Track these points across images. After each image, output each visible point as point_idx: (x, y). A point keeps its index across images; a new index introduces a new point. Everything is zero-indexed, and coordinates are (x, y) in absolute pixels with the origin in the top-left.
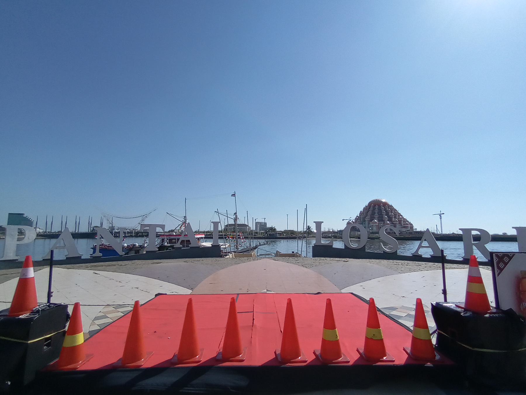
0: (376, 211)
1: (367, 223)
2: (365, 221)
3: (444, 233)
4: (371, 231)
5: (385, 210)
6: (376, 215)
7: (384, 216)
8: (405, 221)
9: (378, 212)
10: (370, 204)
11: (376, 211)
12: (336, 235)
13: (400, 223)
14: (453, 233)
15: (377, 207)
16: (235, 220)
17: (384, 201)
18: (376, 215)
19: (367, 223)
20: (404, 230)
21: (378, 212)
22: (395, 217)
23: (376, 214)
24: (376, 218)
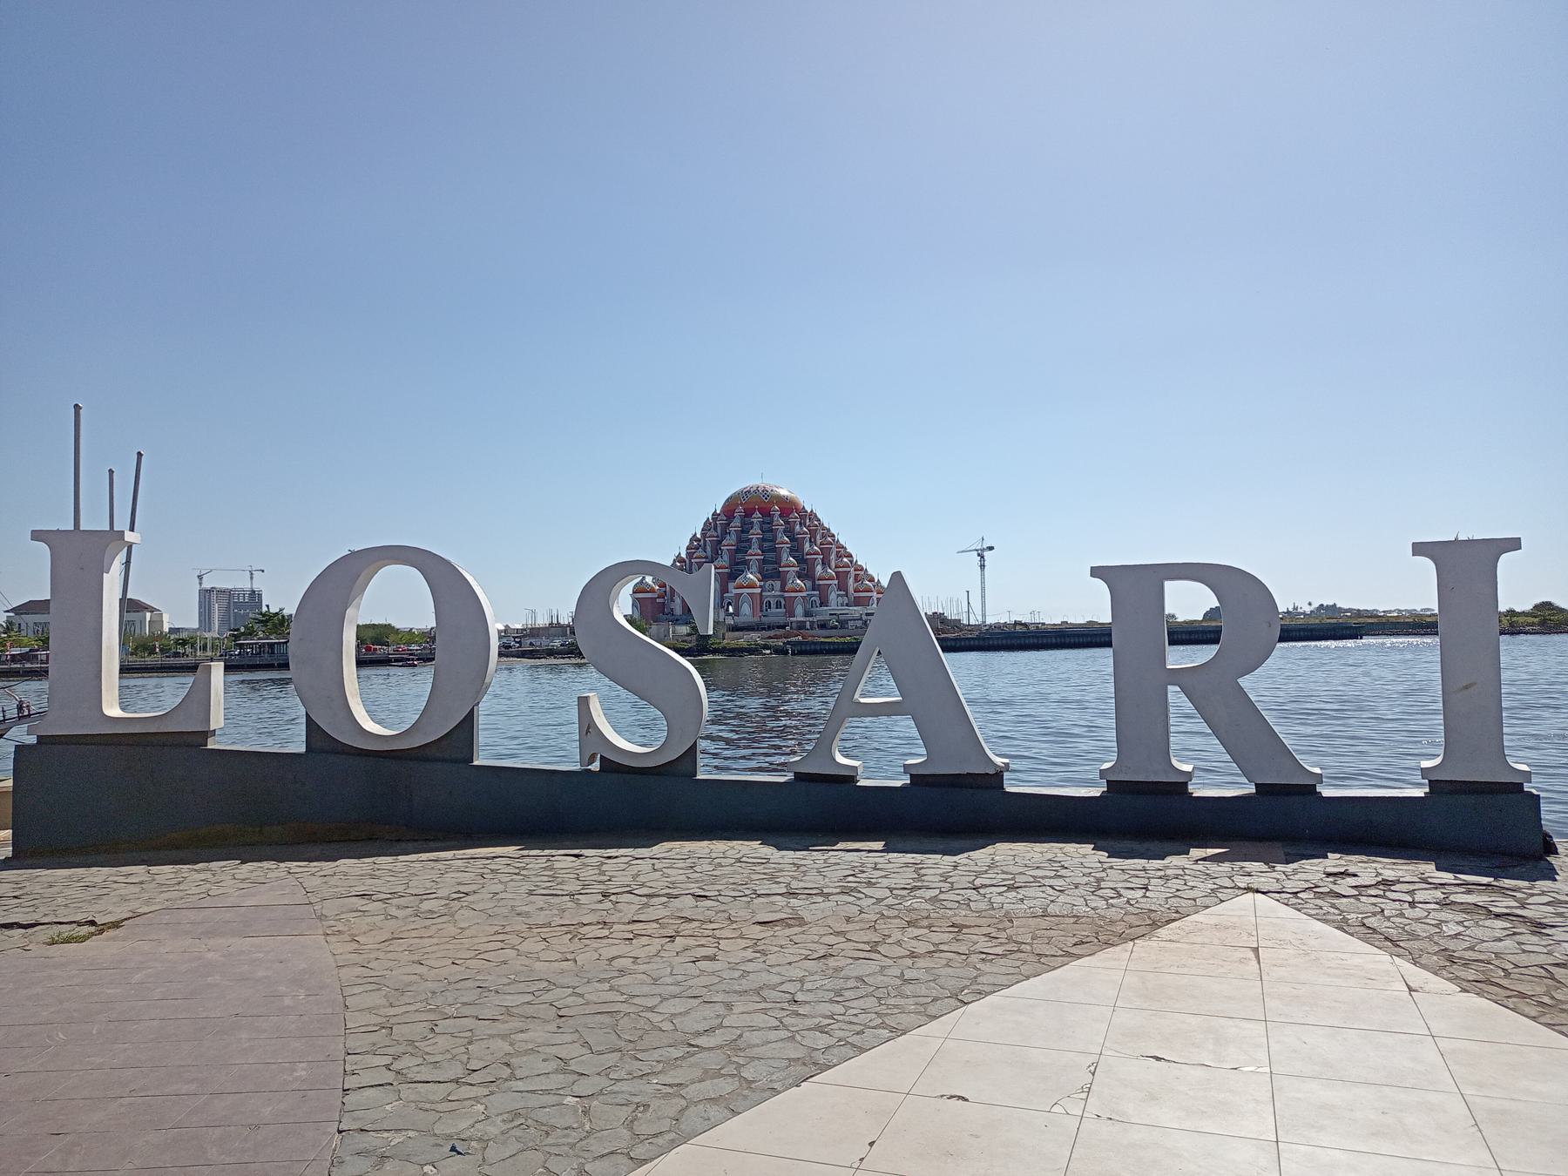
0: (755, 534)
4: (730, 621)
6: (754, 554)
9: (760, 532)
11: (755, 534)
17: (783, 492)
18: (754, 554)
21: (760, 532)
22: (826, 563)
24: (754, 569)
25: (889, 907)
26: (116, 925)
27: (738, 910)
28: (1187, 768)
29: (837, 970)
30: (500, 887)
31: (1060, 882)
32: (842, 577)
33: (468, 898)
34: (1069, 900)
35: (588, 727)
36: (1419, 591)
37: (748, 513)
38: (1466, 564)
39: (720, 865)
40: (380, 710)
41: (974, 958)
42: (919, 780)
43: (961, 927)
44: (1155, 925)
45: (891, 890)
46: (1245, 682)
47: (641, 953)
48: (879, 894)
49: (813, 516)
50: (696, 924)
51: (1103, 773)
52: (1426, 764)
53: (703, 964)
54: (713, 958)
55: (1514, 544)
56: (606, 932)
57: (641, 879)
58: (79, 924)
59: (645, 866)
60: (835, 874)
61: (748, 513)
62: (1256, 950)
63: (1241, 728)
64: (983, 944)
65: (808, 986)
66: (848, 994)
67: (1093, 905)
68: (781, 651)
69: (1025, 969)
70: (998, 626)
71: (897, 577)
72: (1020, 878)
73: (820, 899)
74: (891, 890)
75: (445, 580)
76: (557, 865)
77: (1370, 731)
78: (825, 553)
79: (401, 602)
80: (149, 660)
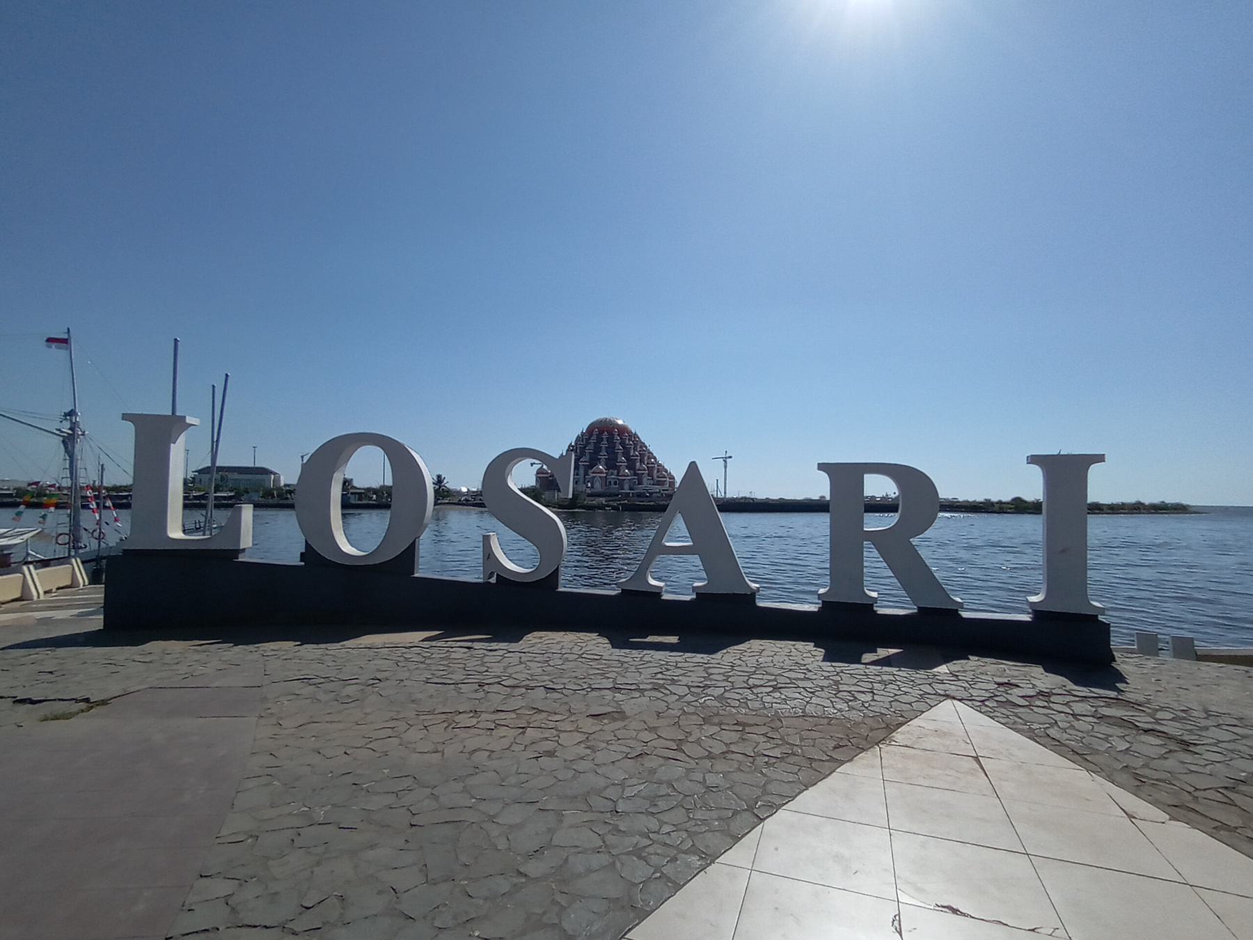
0: (604, 444)
4: (589, 491)
6: (603, 455)
8: (661, 468)
9: (606, 445)
11: (604, 444)
17: (620, 422)
18: (603, 455)
20: (657, 488)
21: (606, 445)
22: (642, 461)
24: (603, 461)
25: (689, 703)
26: (104, 703)
27: (577, 705)
28: (874, 595)
29: (653, 771)
30: (407, 674)
31: (808, 684)
32: (650, 469)
33: (381, 685)
34: (818, 701)
35: (489, 555)
36: (1032, 487)
37: (601, 432)
38: (1066, 472)
39: (567, 660)
40: (351, 541)
41: (761, 761)
42: (702, 596)
43: (745, 725)
44: (891, 728)
45: (689, 687)
46: (915, 541)
47: (497, 746)
48: (682, 691)
49: (636, 435)
50: (544, 715)
51: (820, 596)
52: (1033, 599)
53: (544, 761)
54: (551, 754)
55: (1100, 458)
56: (474, 721)
57: (510, 670)
58: (77, 701)
59: (514, 658)
60: (647, 673)
61: (601, 432)
62: (976, 759)
63: (911, 571)
64: (764, 746)
65: (629, 792)
66: (662, 805)
67: (838, 706)
68: (614, 508)
69: (802, 776)
70: (733, 499)
71: (693, 467)
72: (781, 680)
73: (638, 694)
74: (689, 687)
75: (398, 455)
76: (453, 656)
77: (995, 577)
78: (642, 456)
79: (369, 470)
80: (271, 501)
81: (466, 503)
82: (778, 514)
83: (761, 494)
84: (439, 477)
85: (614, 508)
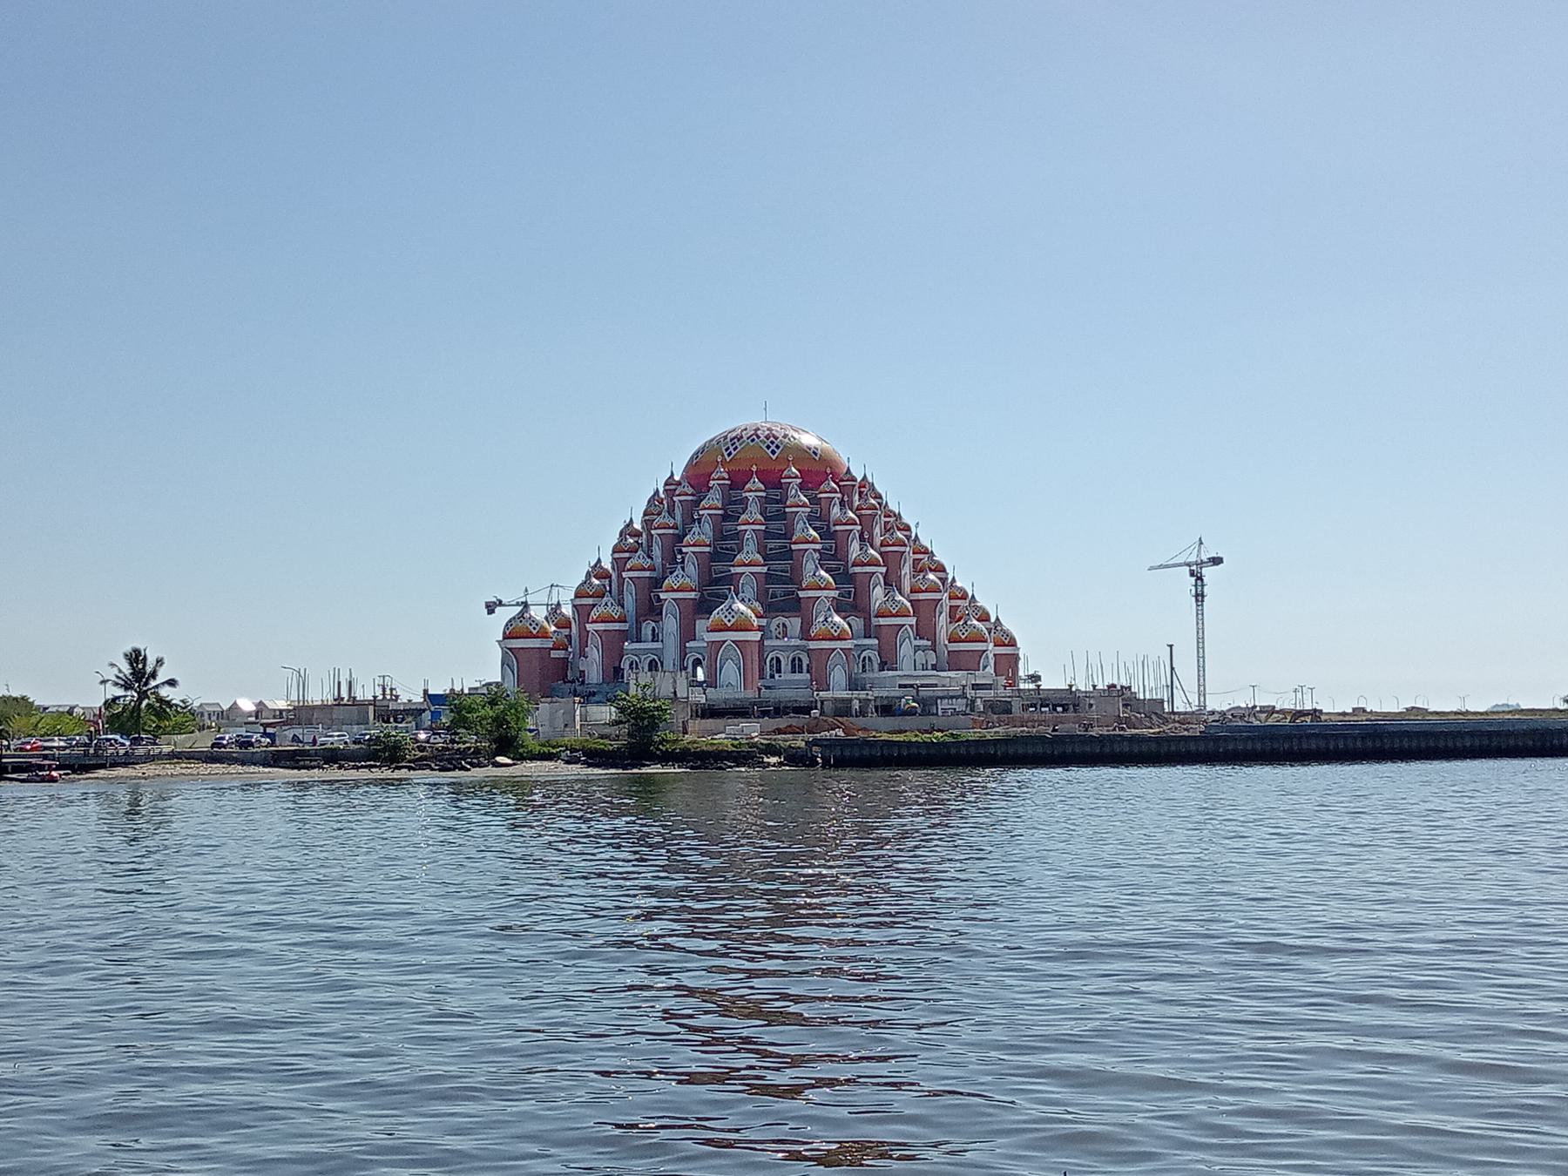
0: (751, 522)
1: (670, 624)
2: (652, 609)
3: (1214, 704)
4: (699, 697)
5: (819, 519)
6: (749, 563)
7: (809, 567)
8: (963, 605)
9: (761, 519)
10: (699, 473)
11: (751, 522)
12: (396, 731)
13: (925, 631)
14: (1120, 694)
15: (754, 490)
16: (1202, 693)
17: (808, 440)
18: (749, 563)
19: (670, 624)
20: (955, 679)
21: (761, 519)
22: (891, 582)
23: (750, 552)
24: (749, 592)
37: (737, 481)
49: (866, 488)
61: (737, 481)
68: (795, 758)
81: (244, 754)
82: (1539, 762)
83: (1335, 698)
84: (135, 657)
85: (795, 758)
